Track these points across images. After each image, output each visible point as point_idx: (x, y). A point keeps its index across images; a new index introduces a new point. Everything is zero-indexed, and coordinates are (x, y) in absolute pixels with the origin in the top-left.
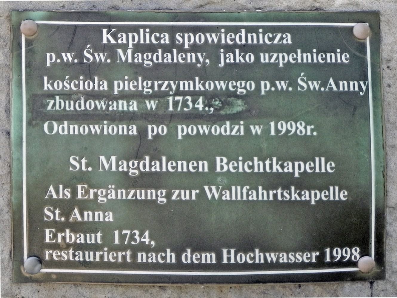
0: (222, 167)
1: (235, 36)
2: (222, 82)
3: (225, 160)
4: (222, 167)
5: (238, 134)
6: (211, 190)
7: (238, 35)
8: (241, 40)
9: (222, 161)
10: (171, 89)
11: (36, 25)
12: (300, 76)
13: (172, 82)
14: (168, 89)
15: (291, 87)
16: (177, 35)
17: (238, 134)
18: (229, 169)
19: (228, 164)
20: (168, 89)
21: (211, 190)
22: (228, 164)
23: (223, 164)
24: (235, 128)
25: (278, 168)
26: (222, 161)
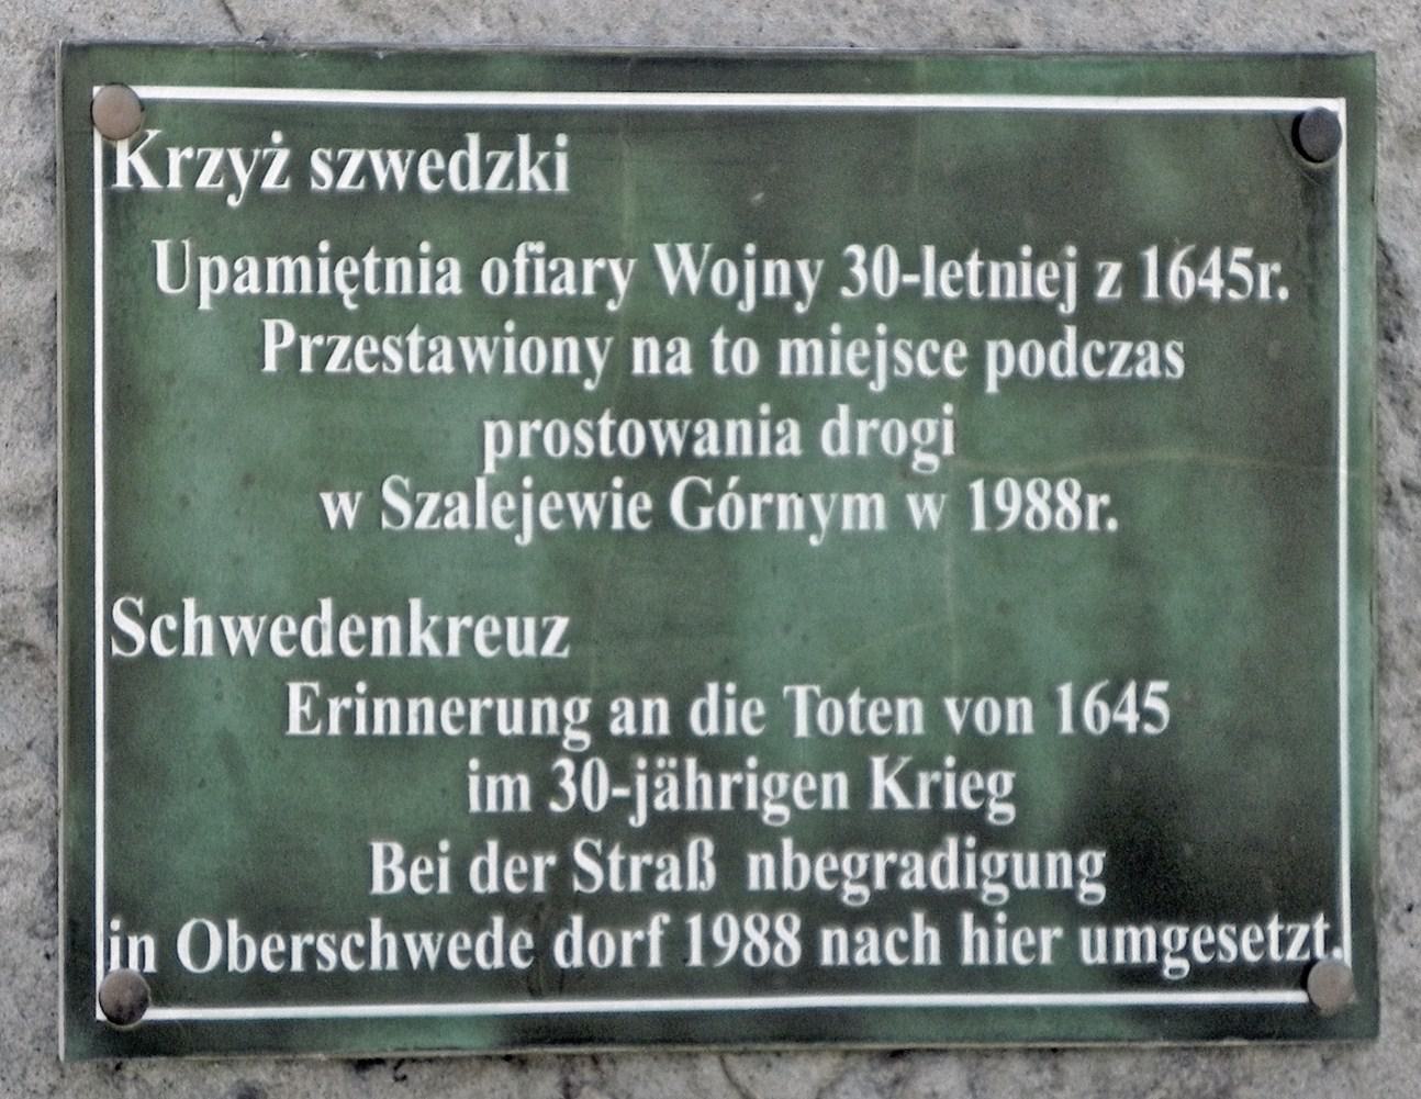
0: (389, 878)
1: (447, 160)
2: (426, 938)
3: (398, 851)
4: (389, 878)
5: (510, 188)
6: (675, 259)
7: (456, 157)
8: (464, 179)
9: (388, 855)
10: (233, 186)
11: (137, 103)
12: (726, 491)
13: (235, 155)
14: (221, 184)
15: (883, 322)
16: (316, 154)
17: (510, 188)
18: (408, 885)
19: (406, 866)
20: (221, 184)
21: (675, 259)
22: (406, 866)
23: (394, 866)
24: (427, 504)
25: (134, 162)
26: (388, 855)
